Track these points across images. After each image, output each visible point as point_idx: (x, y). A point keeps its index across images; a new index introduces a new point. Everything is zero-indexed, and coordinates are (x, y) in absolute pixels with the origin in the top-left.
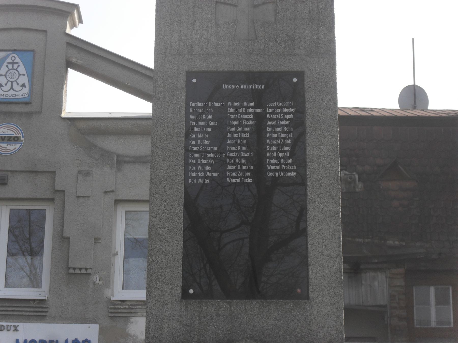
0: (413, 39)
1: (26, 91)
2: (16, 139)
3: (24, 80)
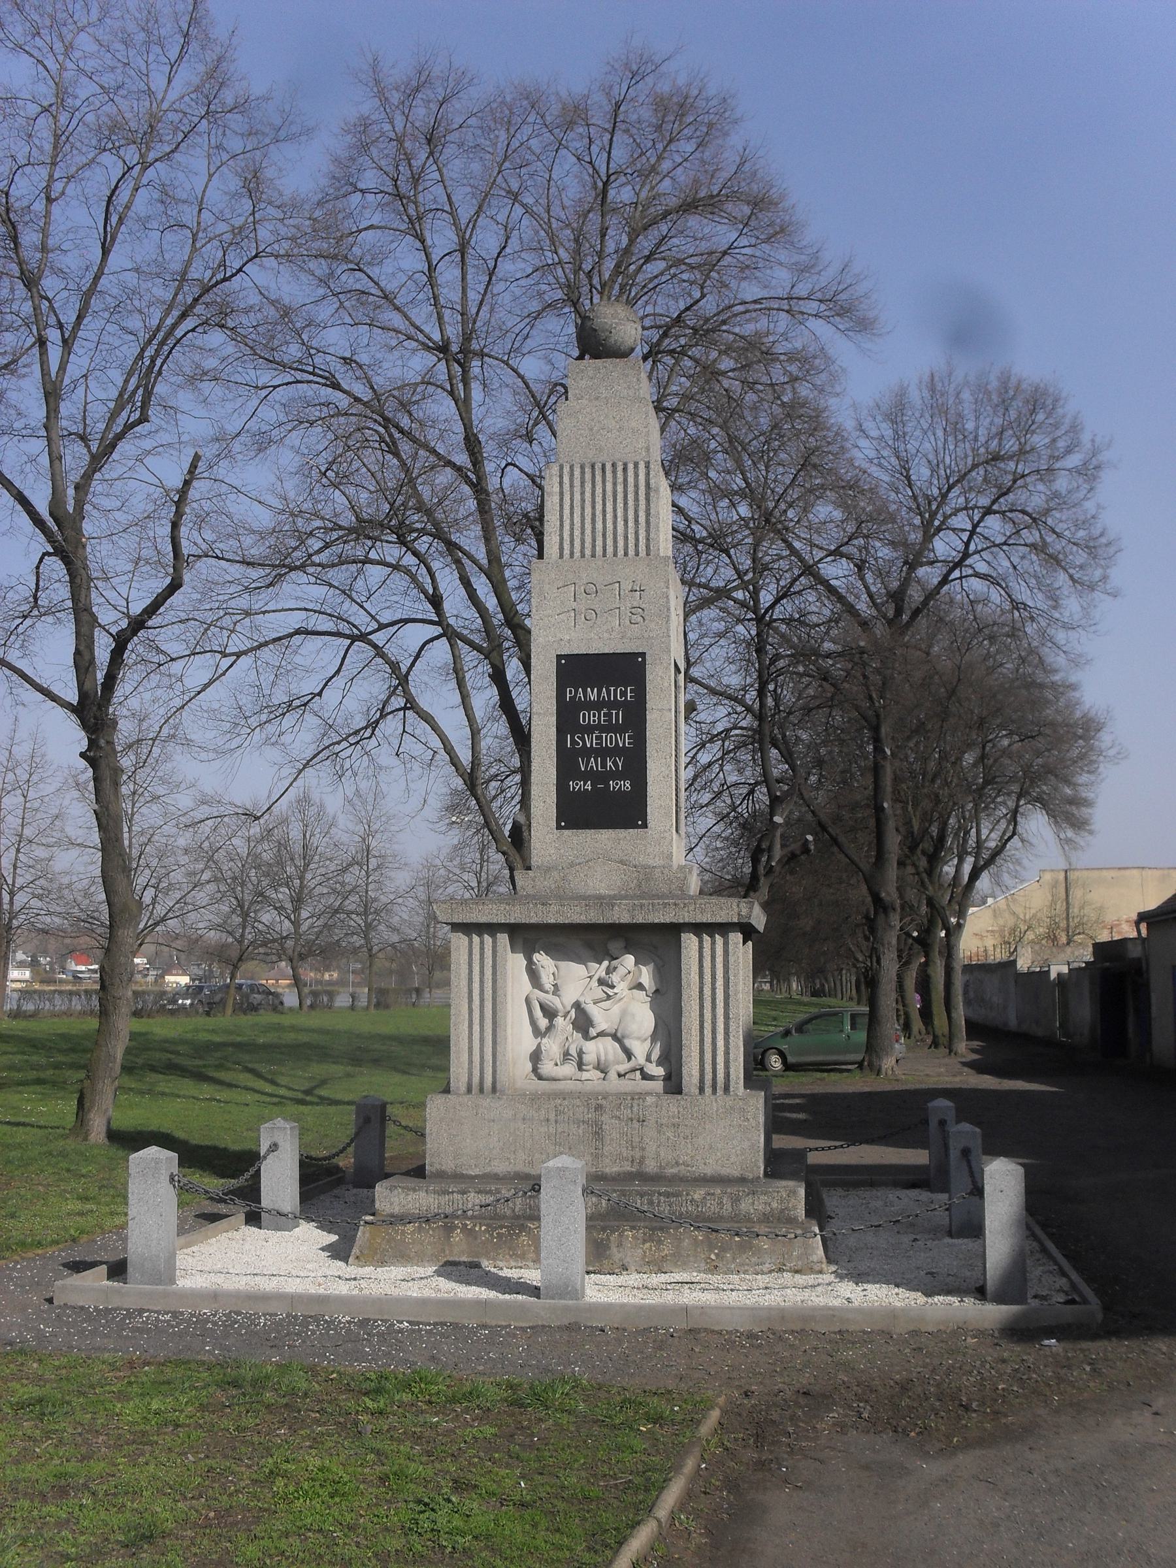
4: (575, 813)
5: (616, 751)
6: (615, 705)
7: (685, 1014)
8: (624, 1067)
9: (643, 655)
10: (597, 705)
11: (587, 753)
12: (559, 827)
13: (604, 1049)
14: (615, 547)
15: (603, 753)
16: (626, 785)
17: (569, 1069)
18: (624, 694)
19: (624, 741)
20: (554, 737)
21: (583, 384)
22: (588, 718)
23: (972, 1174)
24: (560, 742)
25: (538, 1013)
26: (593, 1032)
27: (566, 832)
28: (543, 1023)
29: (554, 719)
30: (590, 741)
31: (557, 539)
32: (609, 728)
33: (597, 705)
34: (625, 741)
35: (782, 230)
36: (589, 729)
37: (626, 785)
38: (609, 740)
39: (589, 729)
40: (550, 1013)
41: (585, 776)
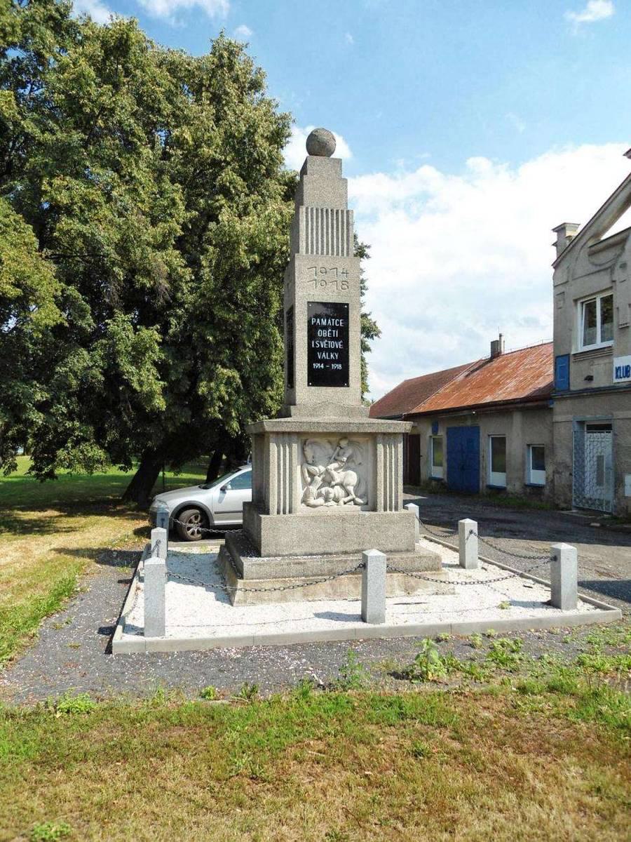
4: (316, 378)
5: (335, 350)
6: (334, 328)
7: (379, 474)
8: (347, 499)
9: (348, 305)
10: (325, 328)
11: (321, 350)
12: (309, 385)
13: (337, 491)
14: (322, 250)
15: (329, 350)
16: (339, 366)
17: (321, 501)
18: (338, 323)
19: (339, 345)
20: (306, 341)
21: (315, 168)
22: (320, 333)
23: (116, 503)
24: (309, 344)
25: (307, 475)
26: (333, 483)
27: (313, 388)
28: (309, 479)
29: (306, 333)
30: (323, 345)
31: (304, 244)
32: (332, 339)
33: (325, 328)
34: (339, 345)
35: (231, 53)
36: (322, 339)
37: (339, 366)
38: (332, 344)
39: (322, 339)
40: (312, 475)
41: (320, 361)
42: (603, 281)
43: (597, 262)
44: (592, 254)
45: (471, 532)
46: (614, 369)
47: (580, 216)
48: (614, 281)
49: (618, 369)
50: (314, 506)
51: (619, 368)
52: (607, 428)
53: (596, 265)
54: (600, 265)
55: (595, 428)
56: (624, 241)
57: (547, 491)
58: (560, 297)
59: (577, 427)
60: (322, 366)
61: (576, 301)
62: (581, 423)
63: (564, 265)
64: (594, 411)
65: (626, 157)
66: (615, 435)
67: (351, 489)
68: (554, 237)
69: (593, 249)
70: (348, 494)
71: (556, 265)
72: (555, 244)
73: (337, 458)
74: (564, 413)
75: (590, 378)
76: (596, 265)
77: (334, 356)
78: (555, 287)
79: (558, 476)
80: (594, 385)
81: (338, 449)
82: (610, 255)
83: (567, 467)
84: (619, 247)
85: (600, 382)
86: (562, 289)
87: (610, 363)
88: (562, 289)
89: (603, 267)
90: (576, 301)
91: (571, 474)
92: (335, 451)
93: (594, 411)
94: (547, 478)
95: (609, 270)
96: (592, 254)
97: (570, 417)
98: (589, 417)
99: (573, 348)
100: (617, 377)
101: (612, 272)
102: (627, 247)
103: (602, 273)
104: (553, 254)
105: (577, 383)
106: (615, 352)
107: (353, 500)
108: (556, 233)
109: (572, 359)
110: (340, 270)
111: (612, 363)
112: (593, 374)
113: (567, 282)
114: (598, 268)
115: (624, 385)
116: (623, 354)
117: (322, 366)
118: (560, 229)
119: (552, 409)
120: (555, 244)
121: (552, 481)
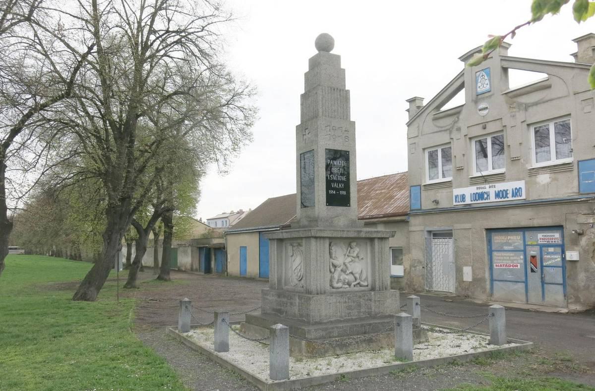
0: (582, 101)
1: (488, 86)
2: (487, 108)
3: (487, 82)
5: (342, 182)
9: (348, 152)
11: (334, 181)
15: (338, 182)
16: (344, 193)
37: (344, 193)
41: (333, 189)
42: (444, 138)
43: (439, 125)
44: (435, 119)
45: (417, 304)
46: (454, 196)
47: (428, 96)
48: (452, 139)
49: (456, 197)
50: (338, 288)
51: (458, 195)
52: (448, 234)
53: (438, 127)
54: (442, 127)
55: (436, 235)
56: (459, 113)
57: (404, 281)
58: (412, 146)
59: (426, 235)
60: (334, 193)
61: (424, 149)
62: (429, 232)
63: (415, 125)
64: (439, 223)
65: (459, 60)
66: (456, 240)
67: (357, 276)
68: (407, 106)
69: (436, 116)
70: (356, 279)
71: (409, 124)
72: (408, 110)
73: (349, 255)
74: (417, 225)
75: (437, 202)
76: (438, 127)
77: (341, 185)
78: (409, 138)
79: (413, 269)
80: (440, 206)
81: (349, 248)
82: (448, 121)
83: (420, 262)
84: (456, 116)
85: (444, 204)
86: (413, 141)
87: (450, 192)
88: (413, 141)
89: (443, 129)
90: (424, 149)
91: (423, 267)
92: (347, 250)
93: (439, 223)
94: (405, 270)
95: (448, 131)
96: (435, 119)
97: (422, 228)
98: (435, 228)
99: (423, 181)
100: (456, 201)
101: (451, 133)
102: (461, 117)
103: (443, 133)
104: (406, 118)
105: (427, 205)
106: (454, 185)
107: (359, 284)
108: (408, 103)
109: (423, 188)
110: (344, 129)
111: (452, 192)
112: (438, 199)
113: (417, 136)
114: (440, 129)
115: (461, 207)
116: (460, 186)
117: (334, 193)
118: (412, 101)
119: (408, 222)
120: (408, 110)
121: (409, 273)
